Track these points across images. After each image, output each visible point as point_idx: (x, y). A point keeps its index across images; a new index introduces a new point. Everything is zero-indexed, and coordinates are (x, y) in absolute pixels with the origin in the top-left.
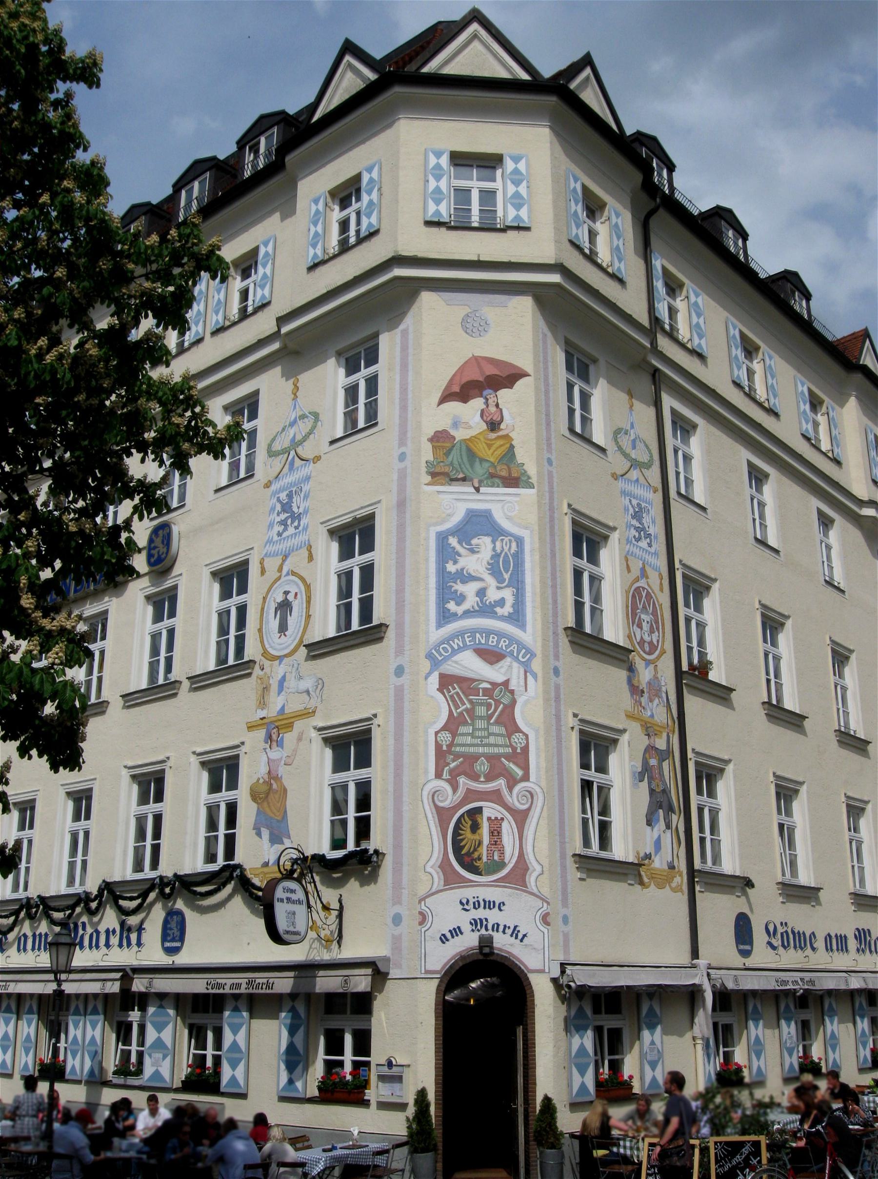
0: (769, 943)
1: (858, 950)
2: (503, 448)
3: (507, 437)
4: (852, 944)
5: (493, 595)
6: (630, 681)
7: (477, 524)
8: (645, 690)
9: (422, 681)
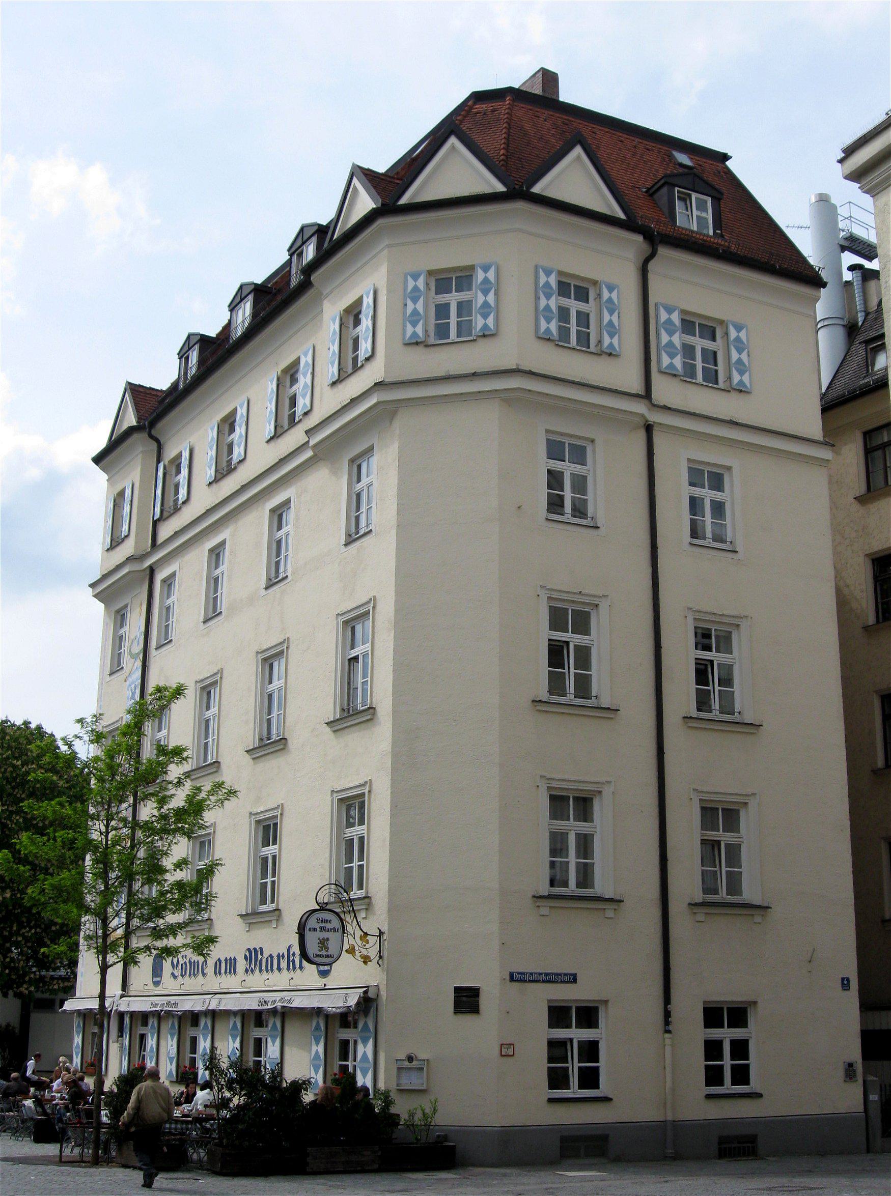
0: (173, 974)
1: (247, 971)
4: (241, 965)
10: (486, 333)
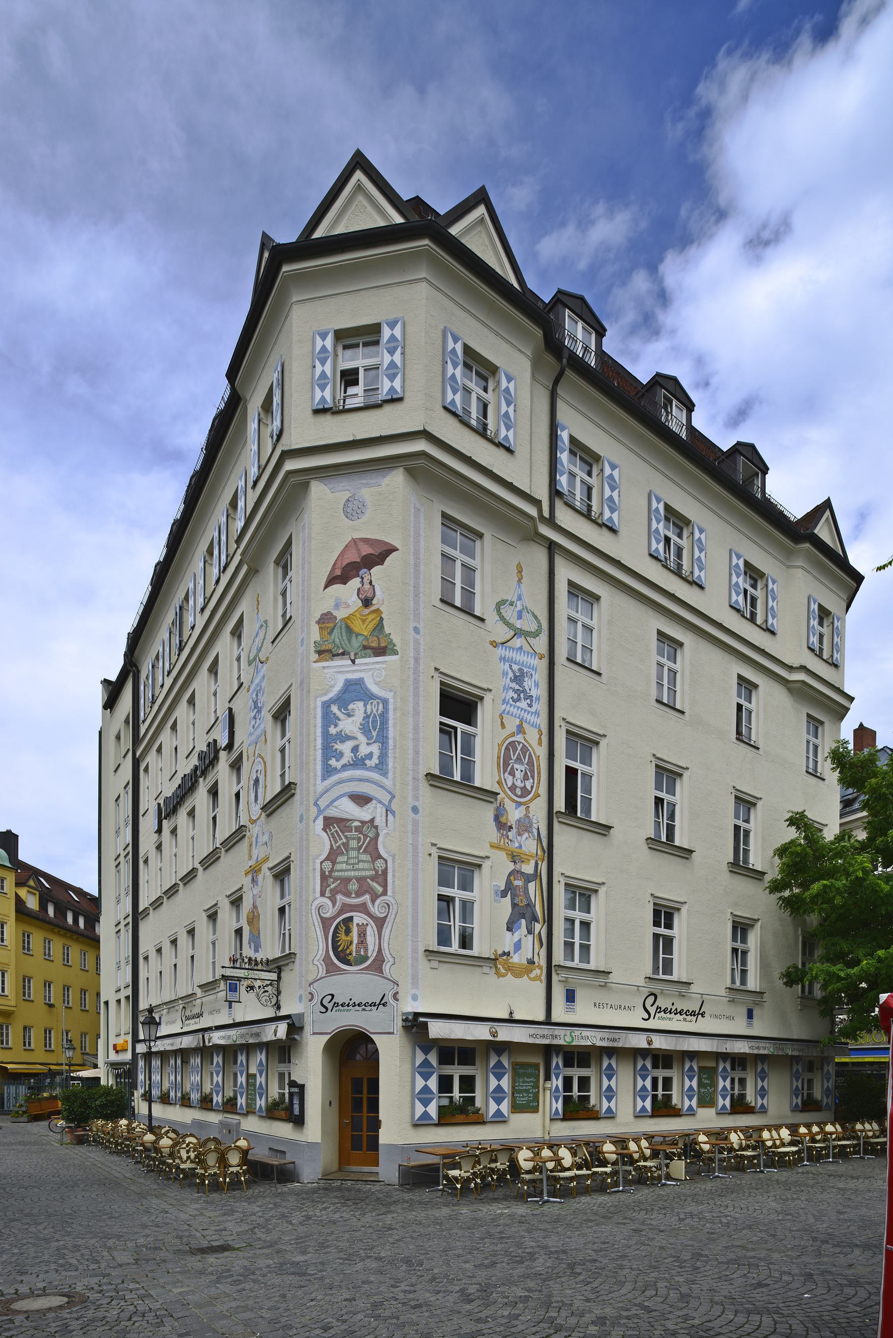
2: (375, 622)
3: (377, 611)
5: (364, 750)
6: (497, 818)
7: (354, 691)
8: (514, 826)
9: (311, 824)
10: (394, 397)
